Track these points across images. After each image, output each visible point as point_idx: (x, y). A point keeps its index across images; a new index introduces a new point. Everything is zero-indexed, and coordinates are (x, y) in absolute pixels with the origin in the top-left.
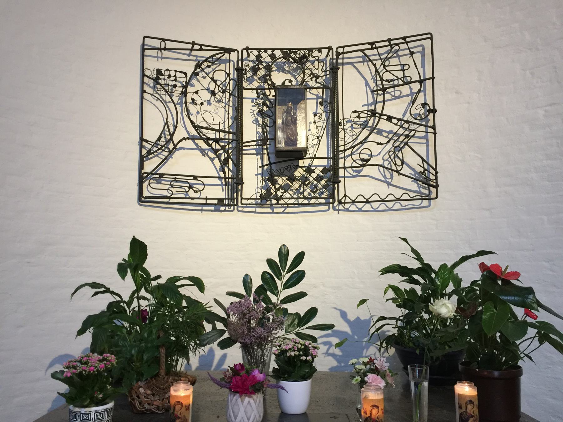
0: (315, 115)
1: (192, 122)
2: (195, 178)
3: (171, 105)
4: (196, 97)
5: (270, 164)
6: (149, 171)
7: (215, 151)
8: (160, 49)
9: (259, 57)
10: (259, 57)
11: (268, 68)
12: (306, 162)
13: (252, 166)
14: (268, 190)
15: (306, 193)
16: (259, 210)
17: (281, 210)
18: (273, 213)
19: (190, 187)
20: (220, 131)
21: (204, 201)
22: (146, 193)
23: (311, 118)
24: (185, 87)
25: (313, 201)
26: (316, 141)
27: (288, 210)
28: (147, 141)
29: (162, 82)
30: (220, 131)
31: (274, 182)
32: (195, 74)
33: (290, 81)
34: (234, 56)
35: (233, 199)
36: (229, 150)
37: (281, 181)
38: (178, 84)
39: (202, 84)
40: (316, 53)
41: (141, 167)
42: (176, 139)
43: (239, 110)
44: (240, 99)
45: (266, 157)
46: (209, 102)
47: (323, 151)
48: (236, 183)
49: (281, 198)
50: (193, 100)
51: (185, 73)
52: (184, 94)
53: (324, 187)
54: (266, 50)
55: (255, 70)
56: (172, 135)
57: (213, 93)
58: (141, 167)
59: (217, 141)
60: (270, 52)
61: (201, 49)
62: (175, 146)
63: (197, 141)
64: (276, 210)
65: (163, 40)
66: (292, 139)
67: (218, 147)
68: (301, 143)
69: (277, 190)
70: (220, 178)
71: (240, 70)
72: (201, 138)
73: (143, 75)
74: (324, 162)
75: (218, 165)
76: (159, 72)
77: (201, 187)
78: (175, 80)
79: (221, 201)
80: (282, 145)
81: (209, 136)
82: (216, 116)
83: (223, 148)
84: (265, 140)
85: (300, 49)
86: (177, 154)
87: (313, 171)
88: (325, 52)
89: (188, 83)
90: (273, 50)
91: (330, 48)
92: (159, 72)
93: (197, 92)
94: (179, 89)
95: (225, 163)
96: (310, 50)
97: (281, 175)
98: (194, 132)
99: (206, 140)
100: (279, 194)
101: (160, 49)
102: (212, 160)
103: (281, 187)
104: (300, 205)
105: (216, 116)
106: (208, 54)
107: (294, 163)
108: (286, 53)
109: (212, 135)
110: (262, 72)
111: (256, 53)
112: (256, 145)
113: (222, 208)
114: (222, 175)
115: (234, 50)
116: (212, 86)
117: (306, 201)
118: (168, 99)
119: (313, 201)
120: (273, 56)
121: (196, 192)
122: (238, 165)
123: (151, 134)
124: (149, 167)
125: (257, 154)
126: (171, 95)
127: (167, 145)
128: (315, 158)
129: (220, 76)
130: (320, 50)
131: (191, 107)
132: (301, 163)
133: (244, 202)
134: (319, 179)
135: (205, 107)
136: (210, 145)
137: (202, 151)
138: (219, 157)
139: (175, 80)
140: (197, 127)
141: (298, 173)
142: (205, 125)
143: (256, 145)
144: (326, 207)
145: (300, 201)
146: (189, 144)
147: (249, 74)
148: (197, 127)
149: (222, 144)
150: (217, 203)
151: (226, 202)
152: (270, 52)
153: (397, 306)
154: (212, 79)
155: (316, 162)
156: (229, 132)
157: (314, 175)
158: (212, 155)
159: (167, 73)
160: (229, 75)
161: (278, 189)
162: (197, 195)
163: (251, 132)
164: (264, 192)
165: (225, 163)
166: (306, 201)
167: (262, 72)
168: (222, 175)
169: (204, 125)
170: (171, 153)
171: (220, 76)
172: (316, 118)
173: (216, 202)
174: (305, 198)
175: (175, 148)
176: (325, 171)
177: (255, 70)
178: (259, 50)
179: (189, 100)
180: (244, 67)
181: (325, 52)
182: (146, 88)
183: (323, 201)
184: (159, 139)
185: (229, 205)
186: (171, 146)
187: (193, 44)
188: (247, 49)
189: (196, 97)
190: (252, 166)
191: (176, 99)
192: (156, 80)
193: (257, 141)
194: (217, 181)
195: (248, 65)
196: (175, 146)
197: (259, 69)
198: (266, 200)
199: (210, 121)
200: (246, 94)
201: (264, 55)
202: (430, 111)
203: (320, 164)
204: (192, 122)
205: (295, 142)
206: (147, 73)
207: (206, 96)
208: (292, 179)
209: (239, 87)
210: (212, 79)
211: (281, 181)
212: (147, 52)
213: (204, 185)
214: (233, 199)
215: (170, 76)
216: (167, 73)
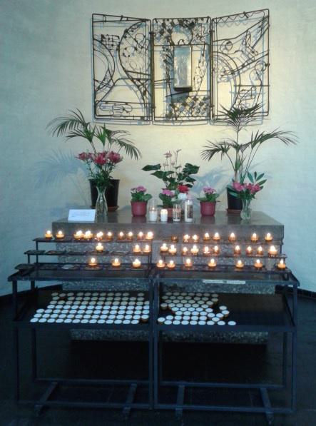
0: (200, 62)
1: (123, 68)
2: (127, 104)
3: (110, 58)
4: (125, 52)
5: (171, 95)
6: (99, 99)
7: (138, 87)
8: (103, 21)
9: (164, 25)
10: (164, 25)
11: (170, 31)
12: (194, 94)
13: (161, 95)
14: (171, 112)
15: (193, 113)
16: (165, 124)
17: (179, 124)
18: (174, 126)
19: (124, 110)
20: (140, 73)
21: (132, 118)
22: (100, 112)
23: (196, 64)
24: (119, 46)
25: (198, 118)
26: (200, 80)
27: (183, 124)
28: (97, 81)
29: (104, 43)
30: (140, 73)
31: (174, 107)
32: (124, 37)
33: (183, 41)
34: (148, 23)
35: (149, 117)
36: (146, 85)
37: (178, 105)
38: (114, 44)
39: (128, 44)
40: (200, 21)
41: (95, 97)
42: (115, 78)
43: (152, 59)
44: (152, 52)
45: (168, 89)
46: (133, 54)
47: (205, 86)
48: (151, 107)
49: (178, 116)
50: (124, 54)
51: (118, 37)
52: (118, 49)
53: (205, 109)
54: (168, 20)
55: (162, 33)
56: (112, 77)
57: (136, 49)
58: (95, 97)
59: (139, 80)
60: (171, 21)
61: (127, 20)
62: (114, 84)
63: (126, 80)
64: (176, 124)
65: (104, 15)
66: (184, 80)
67: (140, 84)
68: (189, 84)
69: (175, 111)
70: (141, 103)
71: (152, 34)
72: (129, 78)
73: (94, 39)
74: (205, 93)
75: (140, 95)
76: (103, 36)
77: (129, 110)
78: (113, 41)
79: (142, 118)
80: (177, 85)
81: (134, 77)
82: (138, 63)
83: (143, 84)
84: (168, 80)
85: (190, 19)
86: (115, 89)
87: (198, 99)
88: (205, 20)
89: (120, 43)
90: (173, 19)
91: (208, 18)
92: (103, 36)
93: (126, 49)
94: (115, 47)
95: (144, 94)
96: (196, 19)
97: (178, 101)
98: (125, 75)
99: (132, 80)
100: (177, 114)
101: (103, 21)
102: (136, 92)
103: (178, 109)
104: (190, 121)
105: (138, 63)
106: (134, 22)
107: (187, 94)
108: (182, 22)
109: (135, 76)
110: (166, 33)
111: (162, 22)
112: (42, 253)
113: (143, 123)
114: (142, 102)
115: (148, 20)
116: (135, 44)
117: (194, 119)
118: (108, 53)
119: (198, 118)
120: (173, 24)
121: (127, 112)
122: (152, 95)
123: (100, 77)
124: (100, 96)
125: (163, 88)
126: (109, 50)
127: (109, 83)
128: (199, 90)
129: (140, 38)
130: (202, 19)
131: (122, 58)
132: (191, 94)
133: (156, 119)
134: (201, 104)
135: (132, 57)
136: (135, 83)
137: (130, 86)
138: (140, 90)
139: (113, 41)
140: (126, 72)
141: (189, 100)
142: (132, 70)
143: (42, 253)
144: (206, 122)
145: (190, 118)
146: (121, 82)
147: (157, 36)
148: (126, 72)
149: (142, 81)
150: (72, 212)
151: (145, 118)
152: (171, 21)
153: (44, 251)
154: (135, 39)
155: (199, 93)
156: (146, 74)
157: (198, 102)
158: (136, 89)
159: (107, 37)
160: (145, 36)
161: (177, 111)
162: (128, 115)
163: (160, 74)
164: (168, 112)
165: (144, 94)
166: (194, 119)
167: (166, 33)
168: (142, 102)
169: (130, 69)
170: (111, 88)
171: (140, 38)
172: (201, 64)
173: (139, 118)
174: (192, 116)
175: (114, 85)
176: (205, 99)
177: (162, 33)
178: (164, 20)
179: (121, 54)
180: (155, 31)
181: (205, 20)
182: (95, 48)
183: (204, 118)
184: (104, 80)
185: (147, 120)
186: (111, 84)
187: (122, 17)
188: (156, 19)
189: (125, 52)
190: (161, 95)
191: (113, 53)
192: (101, 42)
193: (164, 80)
194: (139, 106)
195: (157, 29)
196: (114, 84)
197: (164, 32)
198: (170, 117)
199: (134, 66)
200: (156, 48)
201: (167, 23)
202: (266, 65)
203: (202, 95)
204: (123, 68)
205: (186, 82)
206: (96, 38)
207: (131, 50)
208: (185, 104)
209: (152, 41)
210: (135, 39)
211: (178, 105)
212: (95, 24)
213: (132, 108)
214: (149, 117)
215: (109, 39)
216: (107, 37)
